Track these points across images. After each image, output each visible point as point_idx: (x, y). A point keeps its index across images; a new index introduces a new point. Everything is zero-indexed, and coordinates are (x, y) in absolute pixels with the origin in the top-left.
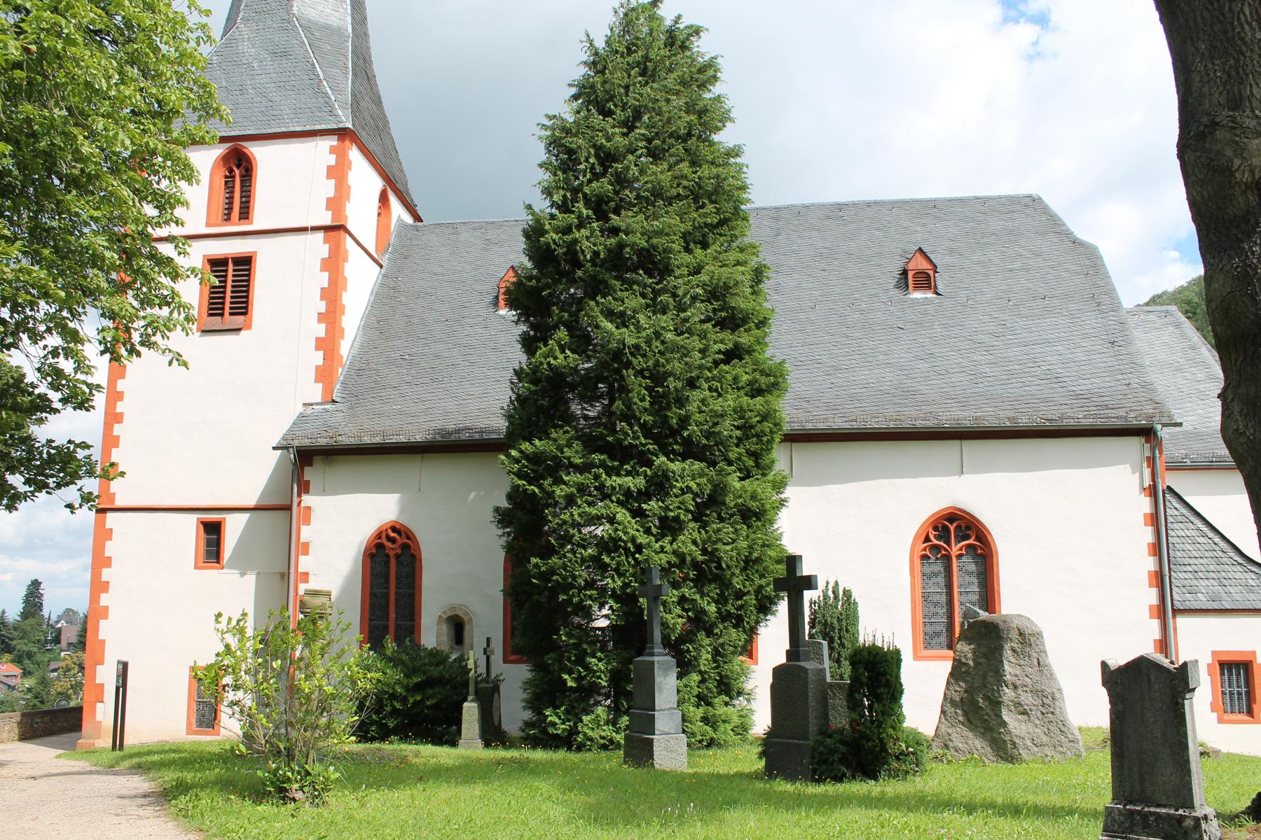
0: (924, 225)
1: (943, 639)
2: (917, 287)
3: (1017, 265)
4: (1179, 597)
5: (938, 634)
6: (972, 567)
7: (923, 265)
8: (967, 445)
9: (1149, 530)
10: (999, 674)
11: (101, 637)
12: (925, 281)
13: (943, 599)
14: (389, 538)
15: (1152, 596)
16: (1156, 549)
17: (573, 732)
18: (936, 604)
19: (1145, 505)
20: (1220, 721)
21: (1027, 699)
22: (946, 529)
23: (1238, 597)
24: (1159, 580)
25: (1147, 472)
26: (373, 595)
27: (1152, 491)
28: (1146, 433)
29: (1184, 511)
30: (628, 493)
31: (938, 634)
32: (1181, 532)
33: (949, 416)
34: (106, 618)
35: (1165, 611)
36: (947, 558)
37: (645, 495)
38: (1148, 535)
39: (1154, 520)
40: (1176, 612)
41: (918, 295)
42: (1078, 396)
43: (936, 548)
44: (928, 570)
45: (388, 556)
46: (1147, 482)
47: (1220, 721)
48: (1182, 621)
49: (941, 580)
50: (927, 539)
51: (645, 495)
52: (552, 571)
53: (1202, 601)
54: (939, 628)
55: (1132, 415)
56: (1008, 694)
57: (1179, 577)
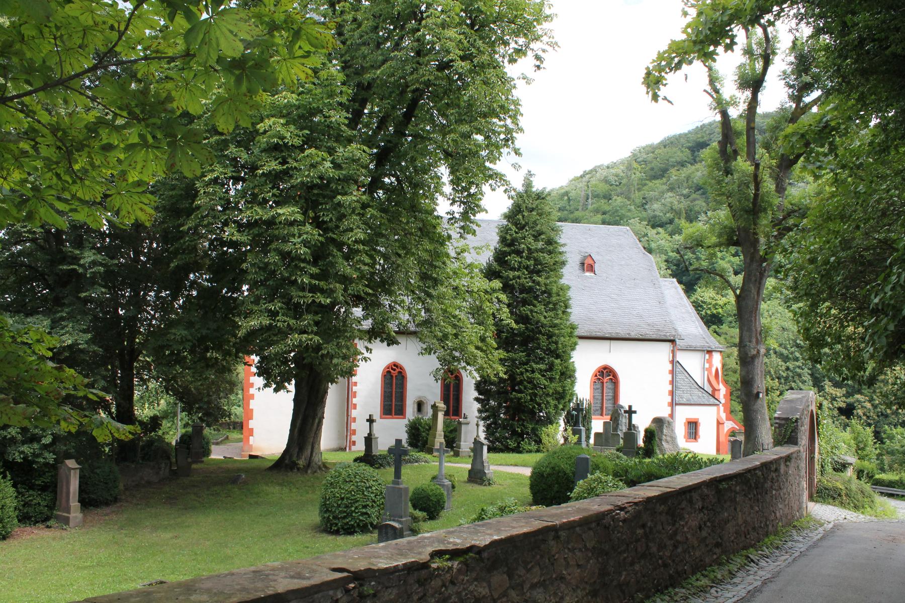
0: (586, 239)
1: (599, 412)
2: (588, 271)
3: (623, 263)
4: (677, 399)
5: (597, 410)
6: (610, 386)
7: (591, 262)
8: (613, 342)
9: (670, 376)
10: (662, 432)
11: (251, 407)
12: (591, 268)
13: (600, 398)
14: (392, 369)
15: (669, 399)
16: (672, 382)
17: (518, 446)
18: (597, 399)
19: (670, 367)
20: (686, 441)
21: (668, 439)
22: (602, 372)
23: (695, 399)
24: (672, 393)
25: (671, 355)
26: (385, 392)
27: (672, 362)
28: (673, 341)
29: (682, 369)
30: (541, 370)
31: (597, 410)
32: (680, 377)
33: (608, 331)
34: (253, 399)
35: (673, 404)
36: (603, 383)
37: (546, 371)
38: (669, 377)
39: (672, 372)
40: (676, 404)
41: (588, 274)
42: (649, 325)
43: (599, 379)
44: (595, 387)
45: (392, 376)
46: (671, 359)
47: (686, 441)
48: (678, 408)
49: (600, 391)
50: (596, 376)
51: (546, 371)
52: (521, 398)
53: (684, 401)
54: (598, 408)
55: (668, 334)
56: (664, 437)
57: (678, 392)
